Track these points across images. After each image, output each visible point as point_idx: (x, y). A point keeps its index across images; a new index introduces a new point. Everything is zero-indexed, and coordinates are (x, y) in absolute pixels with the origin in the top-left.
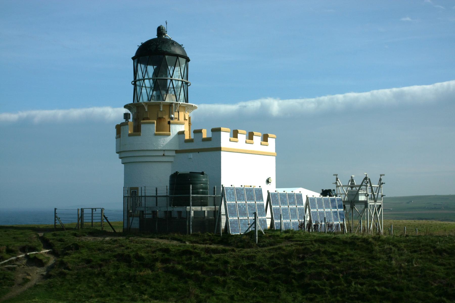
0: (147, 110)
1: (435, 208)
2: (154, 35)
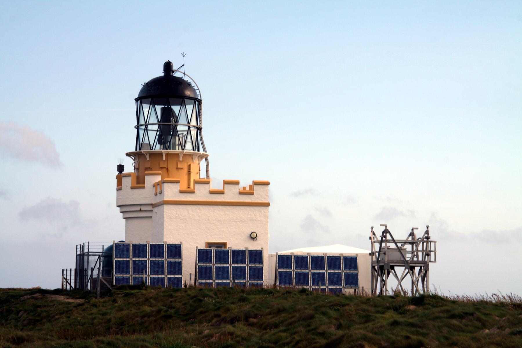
0: (148, 159)
1: (88, 262)
2: (160, 73)
